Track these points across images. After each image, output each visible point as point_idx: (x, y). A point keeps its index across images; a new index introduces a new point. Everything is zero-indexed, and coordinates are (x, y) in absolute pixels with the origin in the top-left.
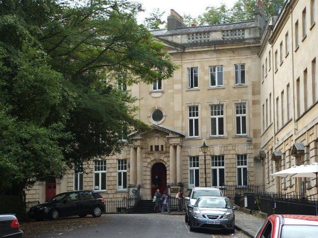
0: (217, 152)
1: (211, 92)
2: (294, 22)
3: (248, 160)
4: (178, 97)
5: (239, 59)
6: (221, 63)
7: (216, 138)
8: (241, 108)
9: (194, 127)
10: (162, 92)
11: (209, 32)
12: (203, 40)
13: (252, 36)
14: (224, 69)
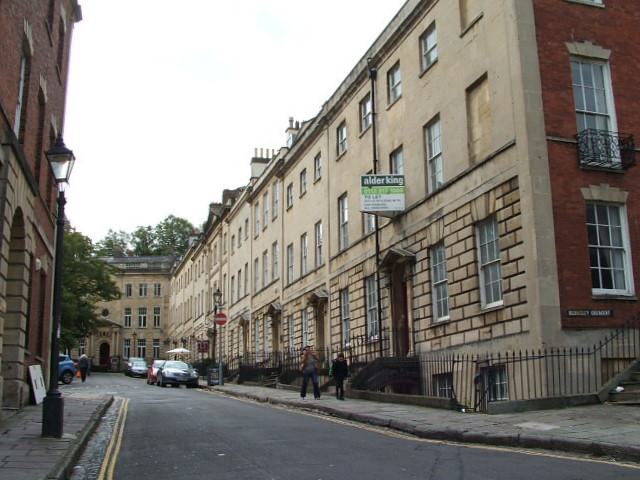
8: (157, 310)
9: (128, 321)
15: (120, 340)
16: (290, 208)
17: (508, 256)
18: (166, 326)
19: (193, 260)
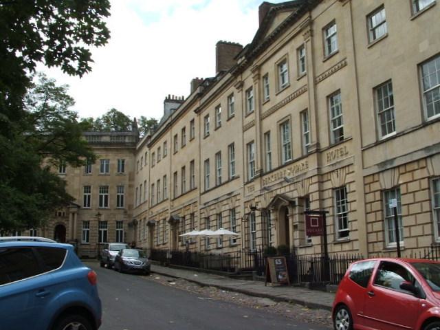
0: (103, 218)
1: (101, 177)
2: (173, 135)
3: (124, 225)
4: (77, 179)
5: (121, 156)
6: (108, 158)
7: (102, 209)
8: (120, 188)
9: (87, 200)
10: (66, 175)
11: (101, 136)
12: (97, 140)
13: (130, 141)
14: (110, 162)
15: (78, 221)
16: (153, 166)
17: (407, 189)
18: (130, 207)
19: (198, 111)
